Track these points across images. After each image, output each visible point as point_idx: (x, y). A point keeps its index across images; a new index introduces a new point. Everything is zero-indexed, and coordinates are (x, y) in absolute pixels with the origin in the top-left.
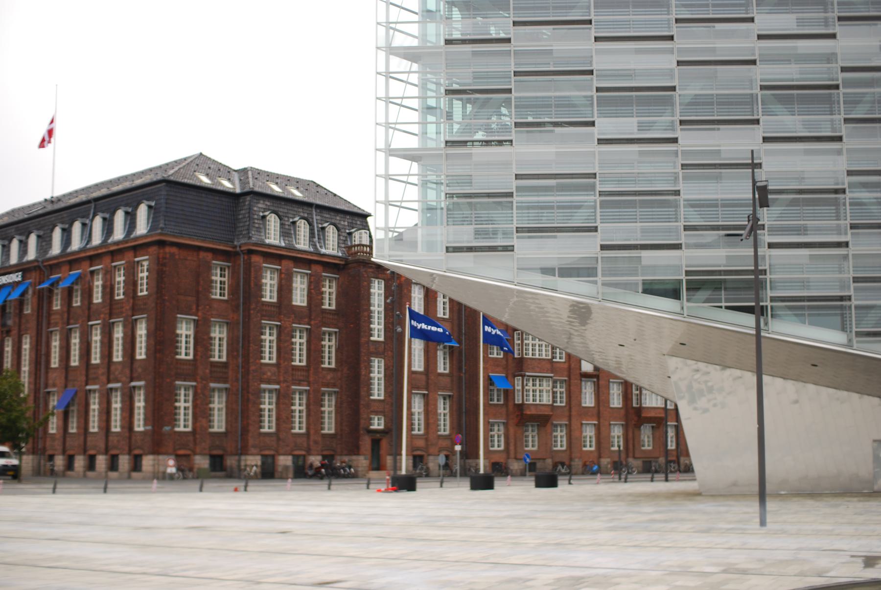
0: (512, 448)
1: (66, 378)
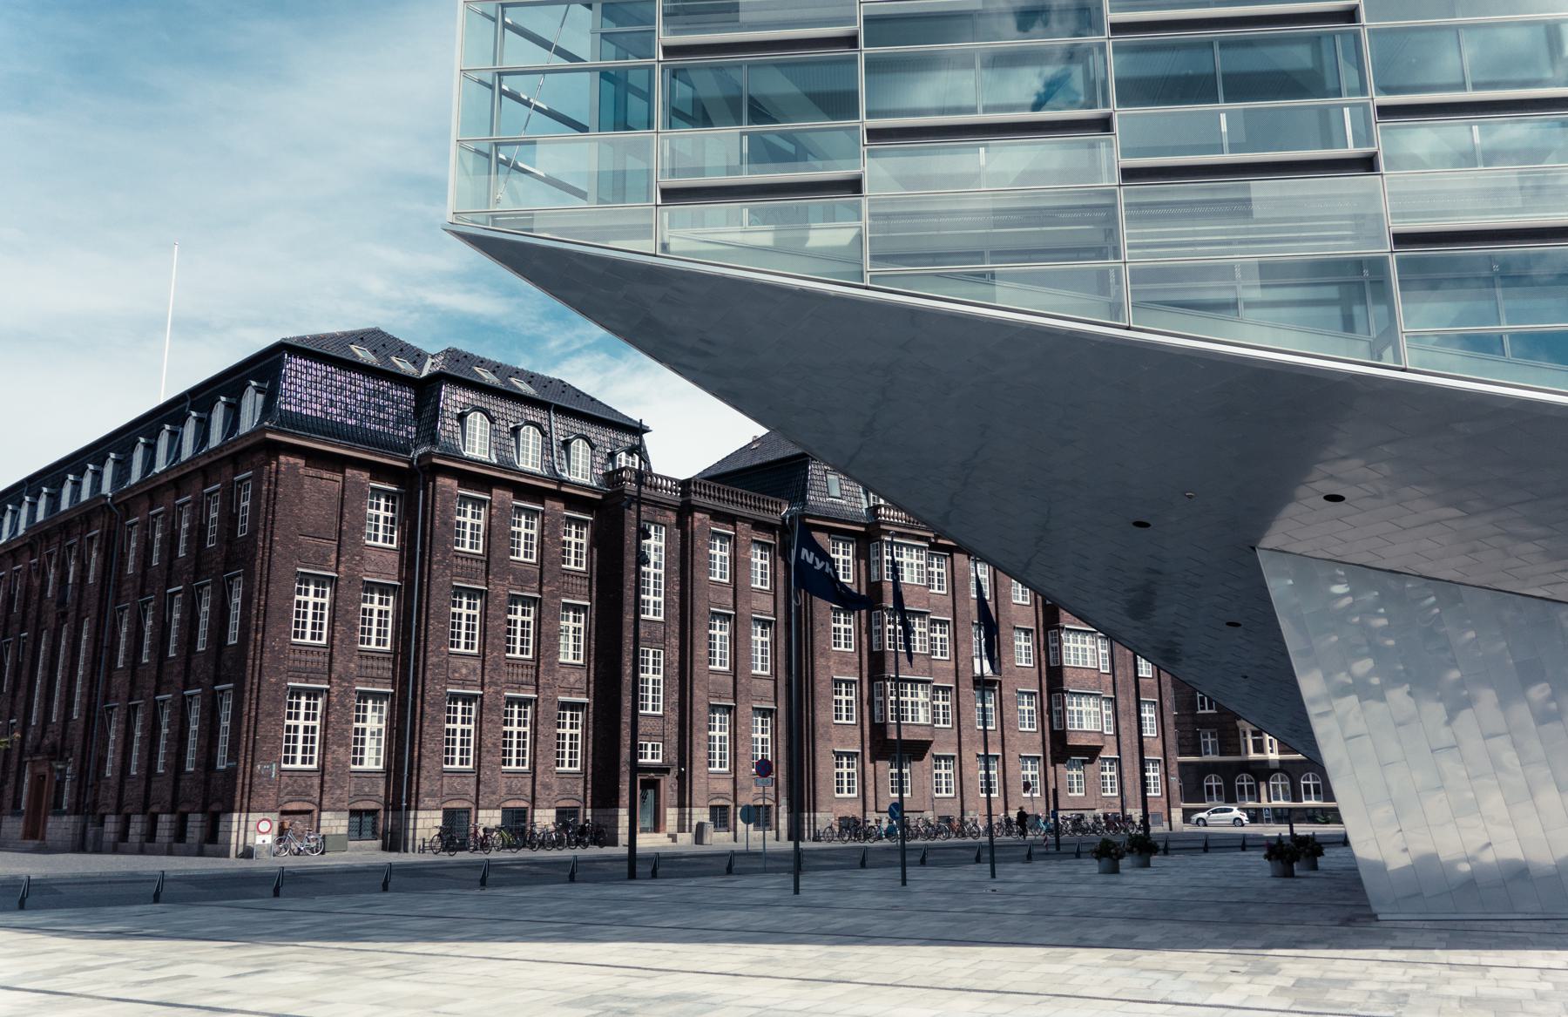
0: (870, 793)
1: (133, 683)
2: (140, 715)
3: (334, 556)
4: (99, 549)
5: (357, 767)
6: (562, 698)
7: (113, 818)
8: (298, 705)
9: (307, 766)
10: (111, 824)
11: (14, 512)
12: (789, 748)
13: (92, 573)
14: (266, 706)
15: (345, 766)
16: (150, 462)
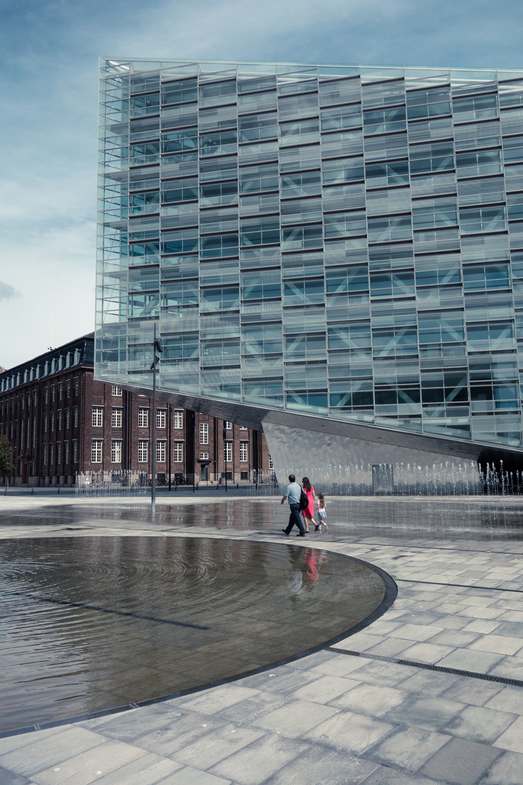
1: (50, 437)
2: (52, 447)
3: (103, 400)
4: (37, 396)
5: (113, 462)
6: (175, 440)
7: (47, 477)
8: (95, 445)
9: (99, 462)
10: (47, 479)
11: (9, 380)
12: (254, 453)
13: (35, 403)
14: (86, 445)
15: (110, 462)
16: (50, 370)
